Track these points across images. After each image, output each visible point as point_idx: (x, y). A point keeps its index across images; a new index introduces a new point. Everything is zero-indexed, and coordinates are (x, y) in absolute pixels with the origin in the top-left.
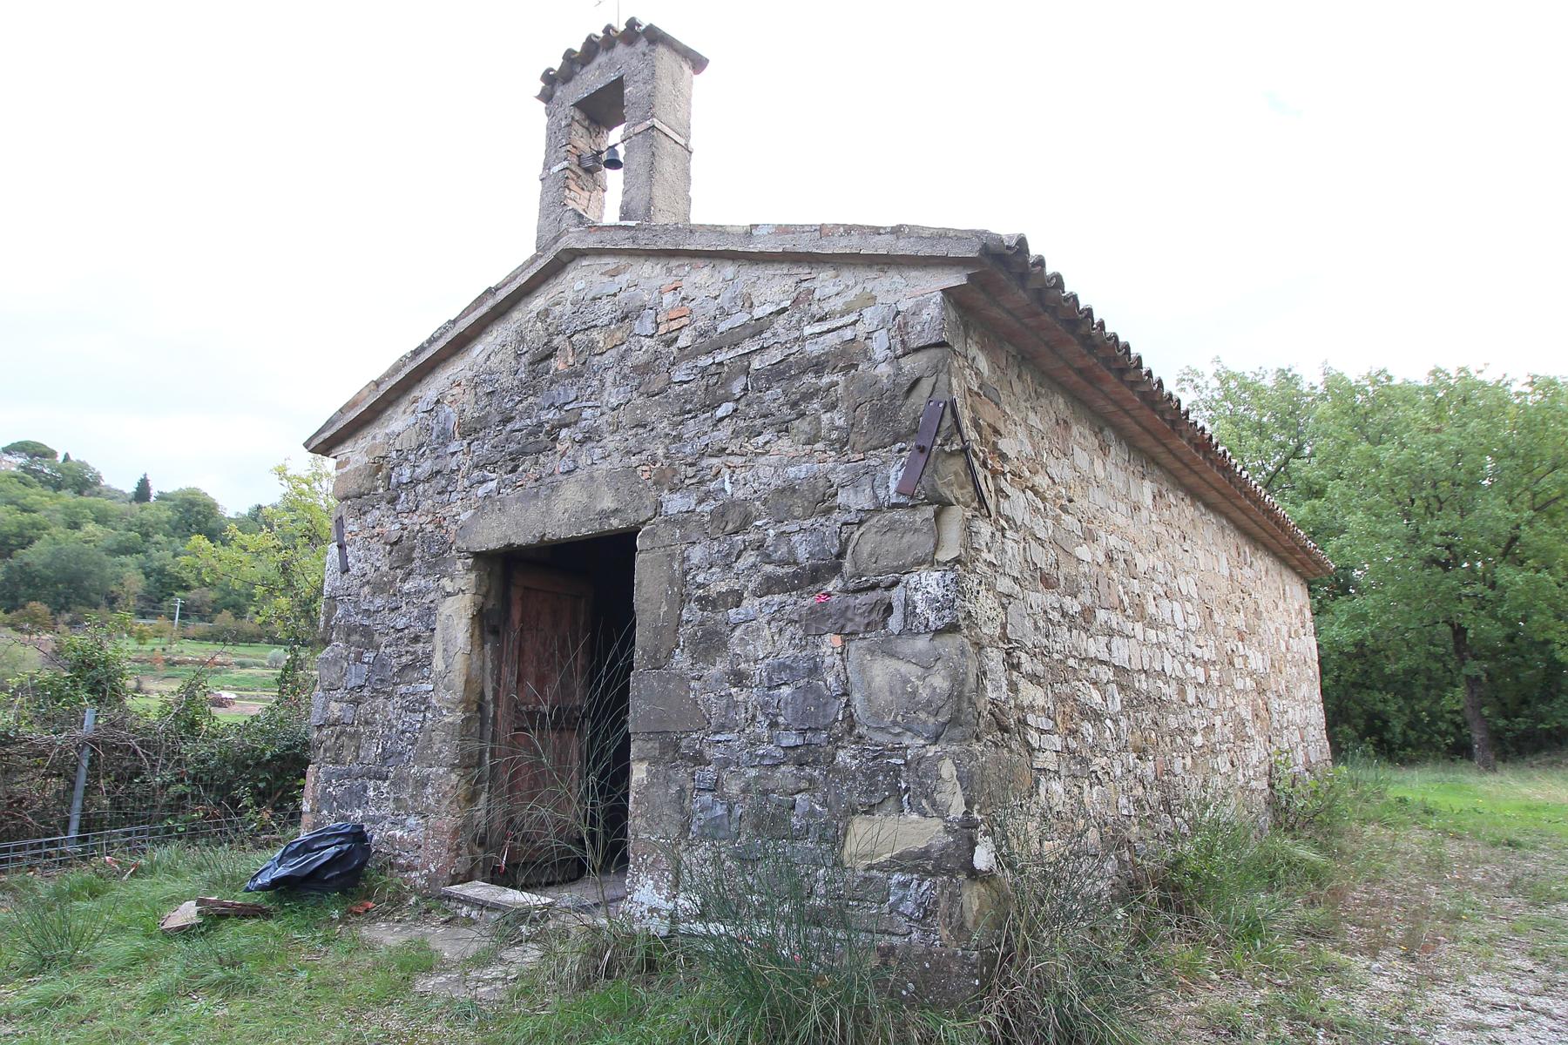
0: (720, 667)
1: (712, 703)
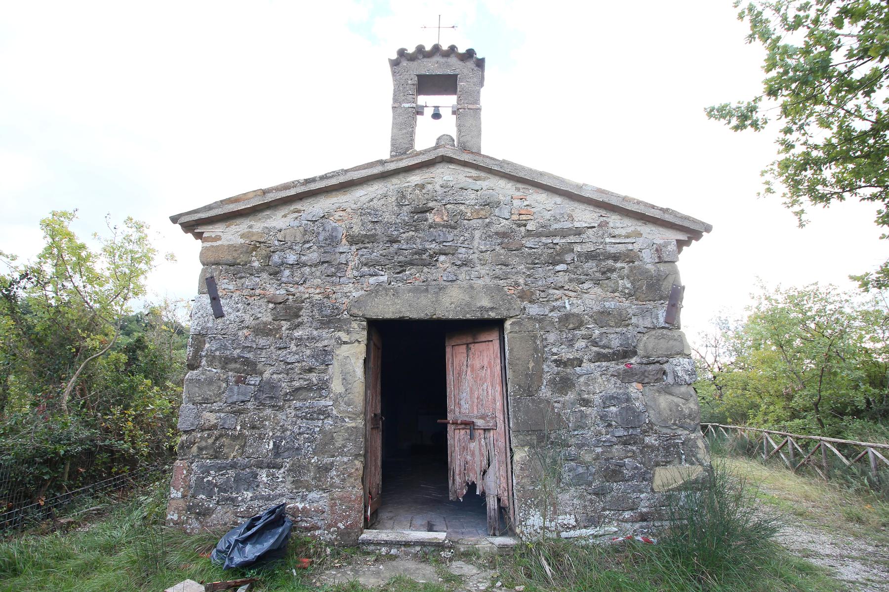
0: (571, 396)
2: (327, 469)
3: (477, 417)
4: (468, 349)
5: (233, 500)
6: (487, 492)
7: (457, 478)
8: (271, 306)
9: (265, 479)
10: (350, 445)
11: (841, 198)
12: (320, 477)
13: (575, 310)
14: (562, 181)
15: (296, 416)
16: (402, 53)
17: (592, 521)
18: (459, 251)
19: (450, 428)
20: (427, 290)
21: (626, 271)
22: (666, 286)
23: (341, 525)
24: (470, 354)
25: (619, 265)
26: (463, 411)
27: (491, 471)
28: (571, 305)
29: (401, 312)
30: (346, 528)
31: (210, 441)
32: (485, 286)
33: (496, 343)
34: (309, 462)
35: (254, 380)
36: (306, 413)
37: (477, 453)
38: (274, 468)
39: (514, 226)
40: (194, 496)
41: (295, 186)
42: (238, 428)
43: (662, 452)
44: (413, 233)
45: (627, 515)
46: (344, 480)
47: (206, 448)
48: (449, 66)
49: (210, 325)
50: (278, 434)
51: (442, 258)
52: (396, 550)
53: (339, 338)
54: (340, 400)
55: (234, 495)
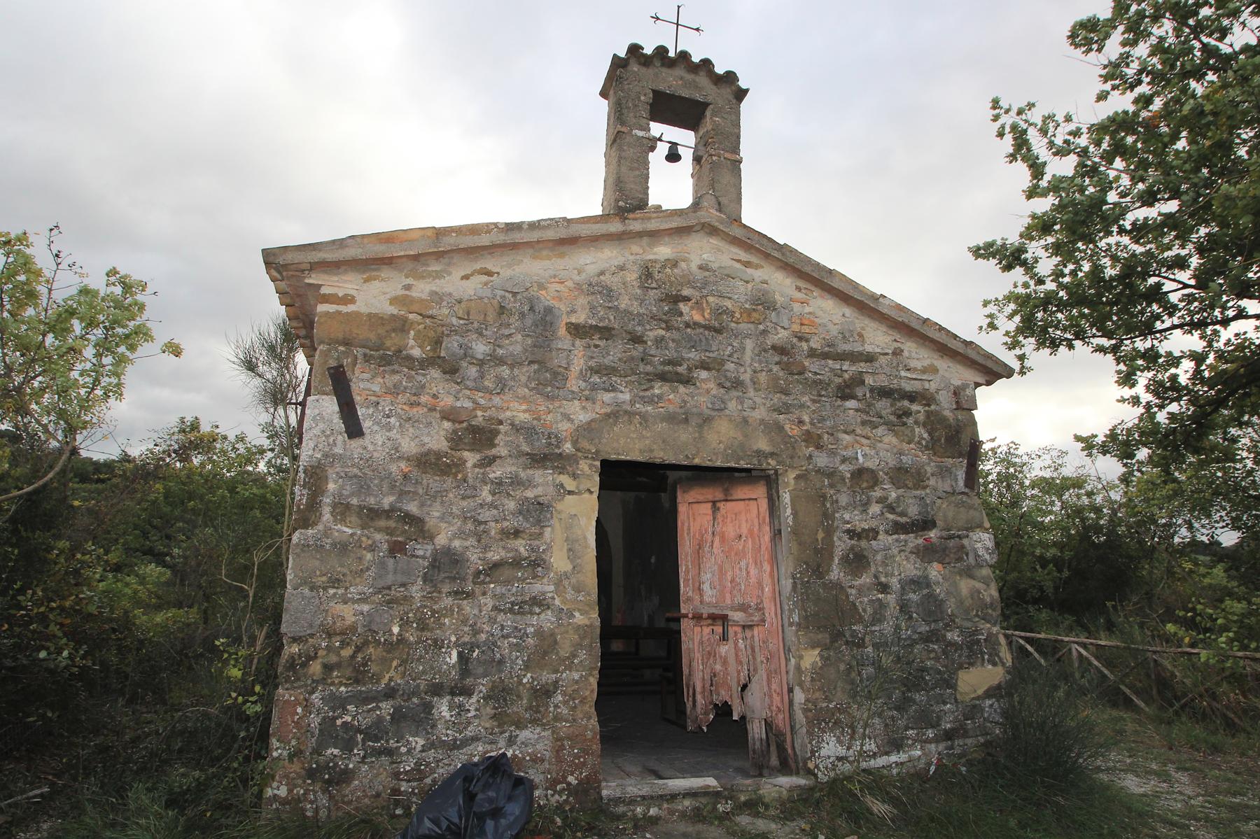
0: (866, 579)
1: (864, 603)
2: (545, 693)
3: (733, 609)
4: (715, 509)
5: (390, 752)
6: (749, 715)
7: (699, 697)
8: (447, 425)
9: (446, 714)
10: (583, 655)
11: (1071, 347)
12: (538, 706)
13: (870, 464)
14: (855, 286)
15: (495, 608)
16: (634, 49)
17: (896, 745)
18: (726, 367)
19: (685, 625)
20: (686, 420)
21: (921, 417)
22: (965, 439)
23: (570, 779)
24: (719, 516)
25: (915, 407)
26: (707, 599)
27: (754, 686)
28: (865, 456)
29: (651, 451)
30: (580, 782)
31: (347, 652)
32: (762, 421)
33: (764, 504)
34: (520, 682)
35: (423, 550)
36: (513, 604)
37: (732, 660)
38: (460, 694)
39: (795, 340)
40: (317, 751)
41: (489, 232)
42: (396, 630)
43: (966, 652)
44: (663, 332)
45: (930, 733)
46: (574, 708)
47: (338, 666)
48: (697, 88)
49: (338, 450)
50: (466, 639)
51: (704, 374)
52: (656, 809)
53: (562, 486)
54: (566, 583)
55: (393, 744)
